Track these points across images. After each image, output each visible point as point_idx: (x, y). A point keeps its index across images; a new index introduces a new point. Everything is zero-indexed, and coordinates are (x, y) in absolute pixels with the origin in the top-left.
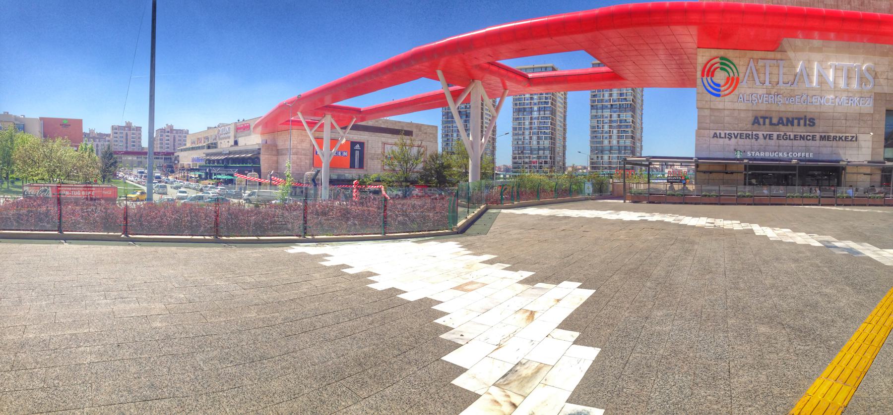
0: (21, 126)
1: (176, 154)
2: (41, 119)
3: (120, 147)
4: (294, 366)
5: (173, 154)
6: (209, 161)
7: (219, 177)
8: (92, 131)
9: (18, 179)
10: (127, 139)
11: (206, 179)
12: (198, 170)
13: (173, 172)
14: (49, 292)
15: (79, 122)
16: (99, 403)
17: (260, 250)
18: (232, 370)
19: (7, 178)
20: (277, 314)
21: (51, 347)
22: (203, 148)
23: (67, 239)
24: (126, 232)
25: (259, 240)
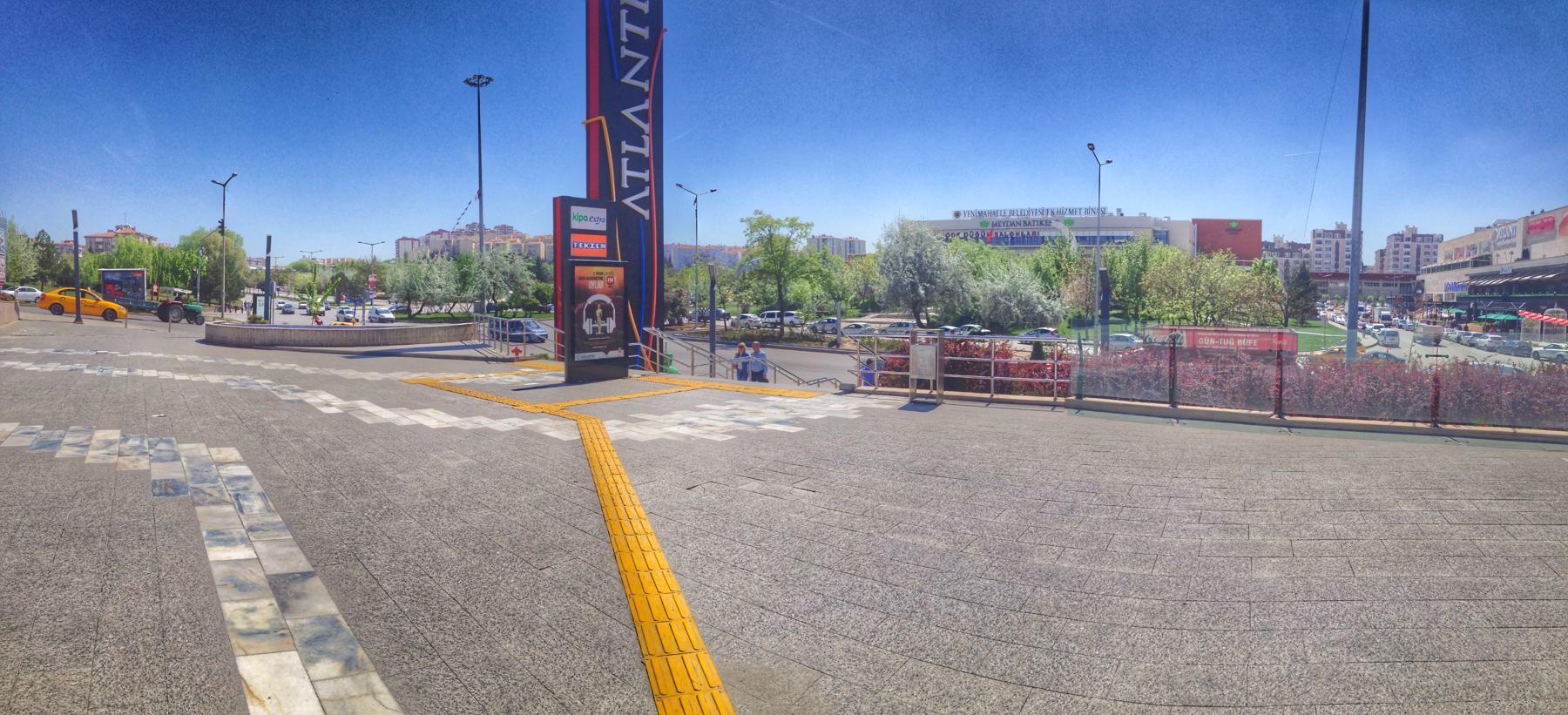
0: (1162, 236)
1: (1419, 278)
2: (1194, 221)
3: (1324, 264)
4: (1492, 688)
5: (1414, 277)
6: (1474, 289)
7: (1492, 316)
8: (1278, 239)
9: (1151, 319)
10: (1337, 252)
11: (1469, 320)
12: (1455, 305)
13: (1412, 309)
14: (1118, 500)
15: (1256, 225)
16: (1118, 695)
17: (1512, 453)
18: (1369, 671)
19: (1136, 317)
20: (1498, 581)
21: (1087, 589)
22: (1464, 265)
23: (1180, 417)
24: (1279, 411)
25: (1515, 434)
